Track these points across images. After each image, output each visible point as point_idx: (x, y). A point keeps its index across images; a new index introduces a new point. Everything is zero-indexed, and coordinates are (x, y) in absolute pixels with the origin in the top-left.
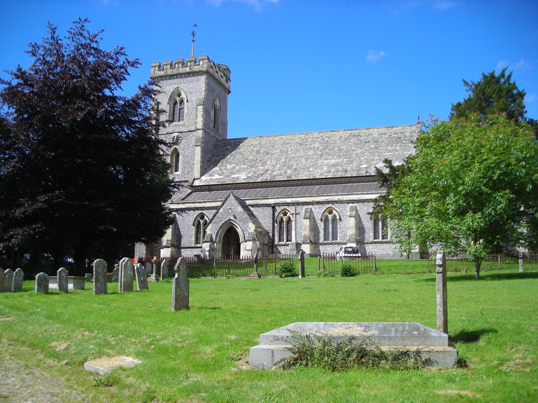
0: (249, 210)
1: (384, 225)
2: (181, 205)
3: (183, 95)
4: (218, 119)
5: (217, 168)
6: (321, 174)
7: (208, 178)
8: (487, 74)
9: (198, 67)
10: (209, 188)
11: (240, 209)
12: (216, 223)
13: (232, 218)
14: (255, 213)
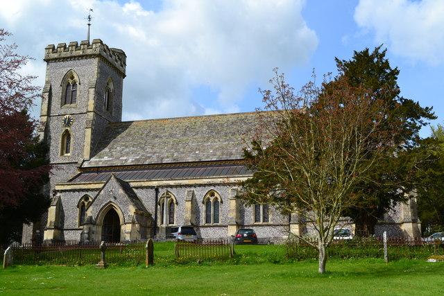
1: (265, 208)
3: (76, 78)
5: (106, 150)
6: (208, 157)
7: (98, 160)
8: (358, 51)
10: (98, 170)
11: (121, 191)
12: (97, 205)
13: (112, 200)
14: (138, 195)
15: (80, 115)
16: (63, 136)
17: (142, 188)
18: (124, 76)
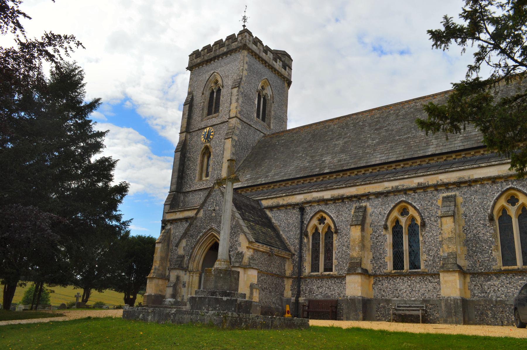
0: (268, 223)
2: (178, 213)
4: (270, 112)
9: (236, 43)
12: (192, 236)
15: (221, 125)
16: (203, 154)
17: (278, 207)
18: (289, 83)
